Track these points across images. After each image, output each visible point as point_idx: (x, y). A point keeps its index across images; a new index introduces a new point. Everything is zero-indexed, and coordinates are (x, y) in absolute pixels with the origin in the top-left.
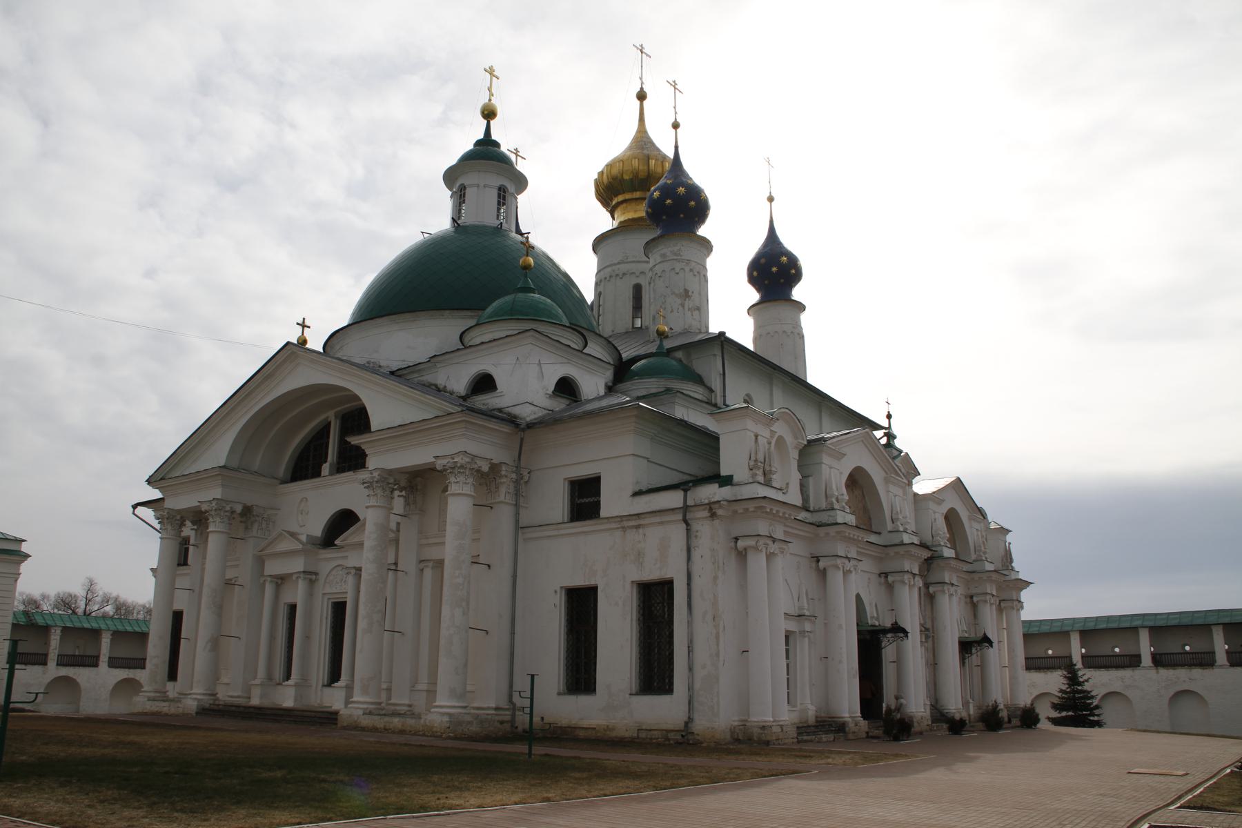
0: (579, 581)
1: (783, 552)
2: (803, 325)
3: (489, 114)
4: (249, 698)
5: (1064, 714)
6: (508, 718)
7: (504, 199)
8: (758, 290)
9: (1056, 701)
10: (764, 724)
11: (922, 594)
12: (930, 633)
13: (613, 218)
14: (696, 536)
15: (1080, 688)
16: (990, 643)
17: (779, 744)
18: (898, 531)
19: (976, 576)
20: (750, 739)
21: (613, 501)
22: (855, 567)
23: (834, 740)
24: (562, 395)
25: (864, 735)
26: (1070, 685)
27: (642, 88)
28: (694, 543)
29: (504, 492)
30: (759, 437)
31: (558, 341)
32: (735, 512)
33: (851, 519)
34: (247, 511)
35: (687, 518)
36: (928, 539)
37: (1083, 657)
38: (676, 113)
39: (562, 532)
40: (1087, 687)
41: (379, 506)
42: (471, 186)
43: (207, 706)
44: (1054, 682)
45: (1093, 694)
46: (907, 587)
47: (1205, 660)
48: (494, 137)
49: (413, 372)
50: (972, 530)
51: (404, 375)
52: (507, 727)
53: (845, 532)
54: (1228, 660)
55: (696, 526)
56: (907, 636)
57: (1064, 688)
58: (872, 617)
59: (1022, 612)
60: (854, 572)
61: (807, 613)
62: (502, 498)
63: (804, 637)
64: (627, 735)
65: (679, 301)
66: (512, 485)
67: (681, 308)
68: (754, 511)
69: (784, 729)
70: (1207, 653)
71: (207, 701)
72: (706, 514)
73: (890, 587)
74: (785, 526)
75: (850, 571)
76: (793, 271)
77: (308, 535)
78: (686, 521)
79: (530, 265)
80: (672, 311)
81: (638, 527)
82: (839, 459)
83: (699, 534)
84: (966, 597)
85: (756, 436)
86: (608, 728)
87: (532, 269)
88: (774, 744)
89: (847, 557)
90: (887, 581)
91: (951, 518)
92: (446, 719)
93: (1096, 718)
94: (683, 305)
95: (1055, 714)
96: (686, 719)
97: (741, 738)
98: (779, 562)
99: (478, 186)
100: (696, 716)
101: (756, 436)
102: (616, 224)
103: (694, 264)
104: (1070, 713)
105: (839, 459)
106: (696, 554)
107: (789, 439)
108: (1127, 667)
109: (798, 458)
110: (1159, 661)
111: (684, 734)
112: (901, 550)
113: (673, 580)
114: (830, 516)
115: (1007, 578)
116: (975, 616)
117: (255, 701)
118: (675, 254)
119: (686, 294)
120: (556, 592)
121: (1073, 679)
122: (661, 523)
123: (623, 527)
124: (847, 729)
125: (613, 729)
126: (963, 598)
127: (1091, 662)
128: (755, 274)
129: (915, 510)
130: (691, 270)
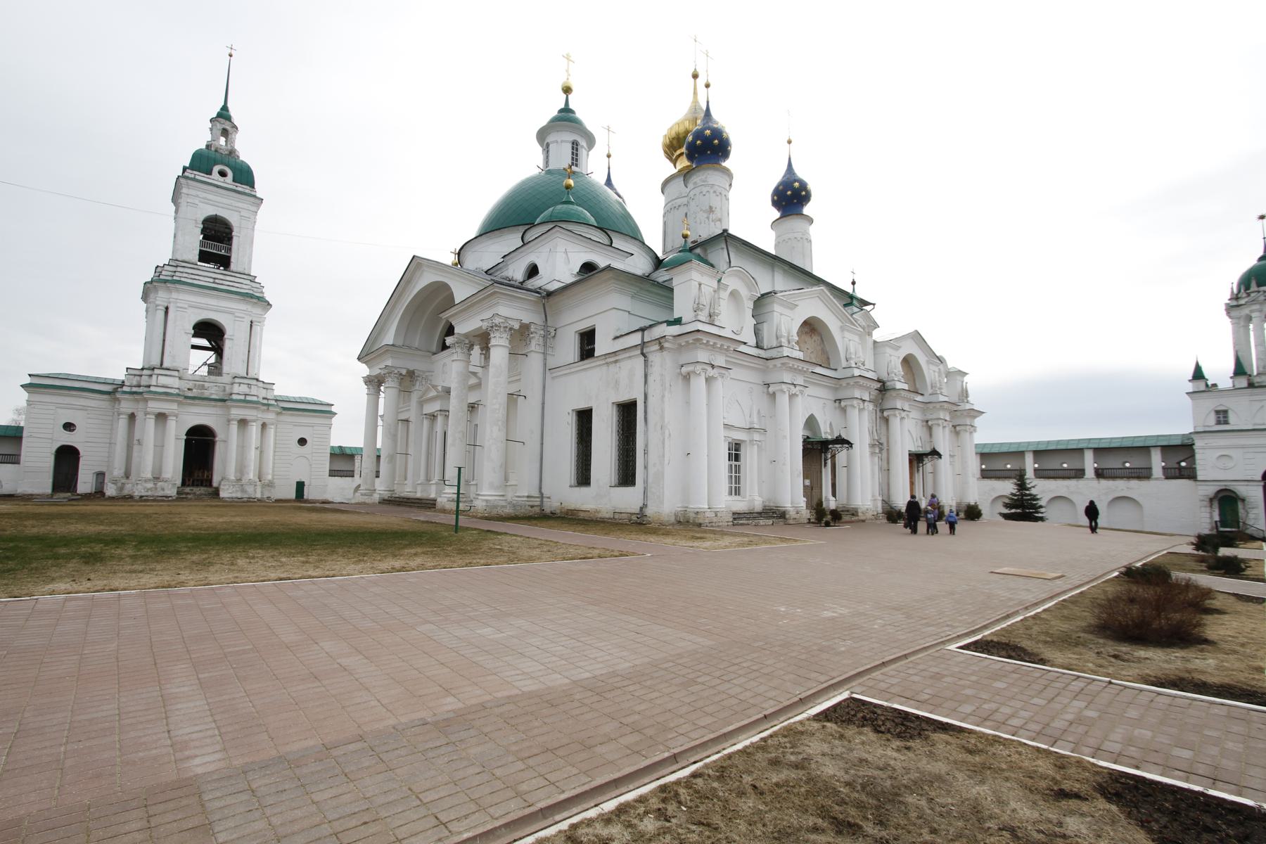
0: (583, 405)
1: (723, 377)
2: (811, 233)
3: (567, 90)
4: (416, 492)
5: (1013, 511)
6: (538, 503)
7: (577, 150)
8: (779, 210)
9: (1007, 501)
10: (698, 510)
11: (878, 417)
12: (881, 447)
13: (675, 167)
14: (651, 365)
15: (1027, 492)
16: (939, 456)
17: (712, 526)
18: (936, 394)
19: (931, 406)
20: (688, 522)
21: (602, 345)
22: (802, 392)
23: (773, 524)
24: (592, 273)
25: (806, 521)
26: (1019, 490)
27: (695, 69)
28: (650, 370)
29: (535, 344)
30: (702, 286)
31: (590, 239)
32: (680, 345)
33: (906, 387)
34: (411, 374)
35: (644, 351)
36: (884, 377)
37: (1036, 470)
38: (708, 75)
39: (572, 370)
40: (1033, 491)
41: (460, 360)
42: (553, 142)
43: (386, 498)
44: (1008, 488)
45: (1038, 497)
46: (941, 427)
47: (1143, 474)
48: (571, 106)
49: (497, 271)
50: (930, 372)
51: (493, 273)
52: (537, 510)
53: (789, 363)
54: (1164, 474)
55: (651, 357)
56: (941, 458)
57: (1014, 491)
58: (826, 433)
59: (976, 435)
60: (800, 396)
61: (756, 426)
62: (533, 348)
63: (753, 445)
64: (607, 516)
65: (705, 215)
66: (541, 339)
67: (707, 221)
68: (780, 367)
69: (719, 514)
70: (1144, 468)
71: (386, 495)
72: (657, 347)
73: (844, 410)
74: (727, 356)
75: (795, 395)
76: (804, 193)
77: (443, 386)
78: (643, 354)
79: (571, 185)
80: (701, 223)
81: (616, 362)
82: (792, 309)
83: (653, 364)
84: (923, 421)
85: (700, 285)
86: (597, 511)
87: (572, 188)
88: (707, 526)
89: (793, 384)
90: (840, 406)
91: (909, 362)
92: (484, 504)
93: (1040, 515)
94: (708, 218)
95: (1006, 511)
96: (641, 505)
97: (681, 520)
98: (719, 385)
99: (557, 142)
100: (649, 503)
101: (700, 285)
102: (676, 171)
103: (717, 187)
104: (1019, 511)
105: (897, 350)
106: (650, 379)
107: (743, 291)
108: (1074, 478)
109: (752, 307)
110: (1100, 474)
111: (639, 516)
112: (851, 382)
113: (636, 401)
114: (778, 352)
115: (959, 408)
116: (931, 435)
117: (419, 495)
118: (704, 181)
119: (711, 210)
120: (569, 413)
121: (1022, 485)
122: (630, 357)
123: (607, 363)
124: (787, 516)
125: (599, 512)
126: (920, 422)
127: (1040, 474)
128: (775, 198)
129: (874, 354)
130: (715, 192)
